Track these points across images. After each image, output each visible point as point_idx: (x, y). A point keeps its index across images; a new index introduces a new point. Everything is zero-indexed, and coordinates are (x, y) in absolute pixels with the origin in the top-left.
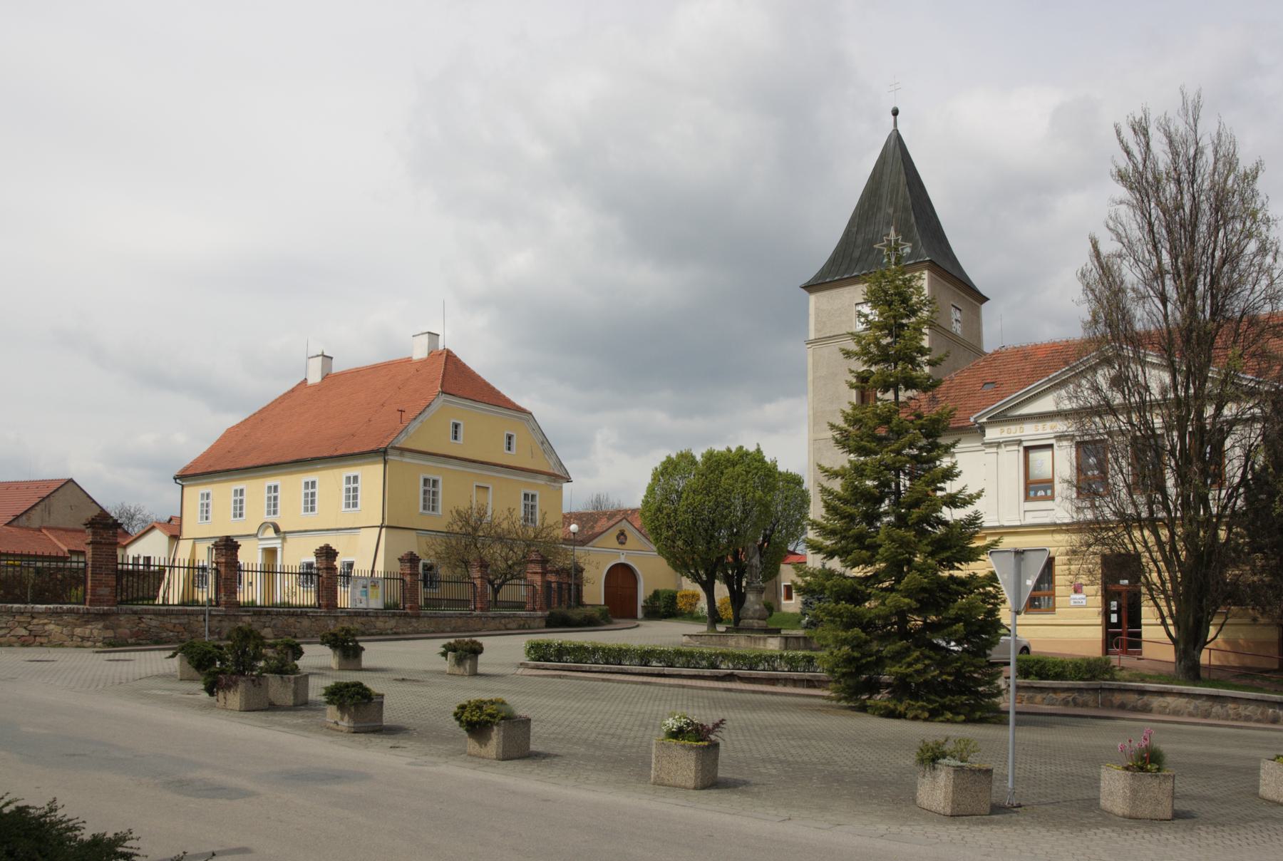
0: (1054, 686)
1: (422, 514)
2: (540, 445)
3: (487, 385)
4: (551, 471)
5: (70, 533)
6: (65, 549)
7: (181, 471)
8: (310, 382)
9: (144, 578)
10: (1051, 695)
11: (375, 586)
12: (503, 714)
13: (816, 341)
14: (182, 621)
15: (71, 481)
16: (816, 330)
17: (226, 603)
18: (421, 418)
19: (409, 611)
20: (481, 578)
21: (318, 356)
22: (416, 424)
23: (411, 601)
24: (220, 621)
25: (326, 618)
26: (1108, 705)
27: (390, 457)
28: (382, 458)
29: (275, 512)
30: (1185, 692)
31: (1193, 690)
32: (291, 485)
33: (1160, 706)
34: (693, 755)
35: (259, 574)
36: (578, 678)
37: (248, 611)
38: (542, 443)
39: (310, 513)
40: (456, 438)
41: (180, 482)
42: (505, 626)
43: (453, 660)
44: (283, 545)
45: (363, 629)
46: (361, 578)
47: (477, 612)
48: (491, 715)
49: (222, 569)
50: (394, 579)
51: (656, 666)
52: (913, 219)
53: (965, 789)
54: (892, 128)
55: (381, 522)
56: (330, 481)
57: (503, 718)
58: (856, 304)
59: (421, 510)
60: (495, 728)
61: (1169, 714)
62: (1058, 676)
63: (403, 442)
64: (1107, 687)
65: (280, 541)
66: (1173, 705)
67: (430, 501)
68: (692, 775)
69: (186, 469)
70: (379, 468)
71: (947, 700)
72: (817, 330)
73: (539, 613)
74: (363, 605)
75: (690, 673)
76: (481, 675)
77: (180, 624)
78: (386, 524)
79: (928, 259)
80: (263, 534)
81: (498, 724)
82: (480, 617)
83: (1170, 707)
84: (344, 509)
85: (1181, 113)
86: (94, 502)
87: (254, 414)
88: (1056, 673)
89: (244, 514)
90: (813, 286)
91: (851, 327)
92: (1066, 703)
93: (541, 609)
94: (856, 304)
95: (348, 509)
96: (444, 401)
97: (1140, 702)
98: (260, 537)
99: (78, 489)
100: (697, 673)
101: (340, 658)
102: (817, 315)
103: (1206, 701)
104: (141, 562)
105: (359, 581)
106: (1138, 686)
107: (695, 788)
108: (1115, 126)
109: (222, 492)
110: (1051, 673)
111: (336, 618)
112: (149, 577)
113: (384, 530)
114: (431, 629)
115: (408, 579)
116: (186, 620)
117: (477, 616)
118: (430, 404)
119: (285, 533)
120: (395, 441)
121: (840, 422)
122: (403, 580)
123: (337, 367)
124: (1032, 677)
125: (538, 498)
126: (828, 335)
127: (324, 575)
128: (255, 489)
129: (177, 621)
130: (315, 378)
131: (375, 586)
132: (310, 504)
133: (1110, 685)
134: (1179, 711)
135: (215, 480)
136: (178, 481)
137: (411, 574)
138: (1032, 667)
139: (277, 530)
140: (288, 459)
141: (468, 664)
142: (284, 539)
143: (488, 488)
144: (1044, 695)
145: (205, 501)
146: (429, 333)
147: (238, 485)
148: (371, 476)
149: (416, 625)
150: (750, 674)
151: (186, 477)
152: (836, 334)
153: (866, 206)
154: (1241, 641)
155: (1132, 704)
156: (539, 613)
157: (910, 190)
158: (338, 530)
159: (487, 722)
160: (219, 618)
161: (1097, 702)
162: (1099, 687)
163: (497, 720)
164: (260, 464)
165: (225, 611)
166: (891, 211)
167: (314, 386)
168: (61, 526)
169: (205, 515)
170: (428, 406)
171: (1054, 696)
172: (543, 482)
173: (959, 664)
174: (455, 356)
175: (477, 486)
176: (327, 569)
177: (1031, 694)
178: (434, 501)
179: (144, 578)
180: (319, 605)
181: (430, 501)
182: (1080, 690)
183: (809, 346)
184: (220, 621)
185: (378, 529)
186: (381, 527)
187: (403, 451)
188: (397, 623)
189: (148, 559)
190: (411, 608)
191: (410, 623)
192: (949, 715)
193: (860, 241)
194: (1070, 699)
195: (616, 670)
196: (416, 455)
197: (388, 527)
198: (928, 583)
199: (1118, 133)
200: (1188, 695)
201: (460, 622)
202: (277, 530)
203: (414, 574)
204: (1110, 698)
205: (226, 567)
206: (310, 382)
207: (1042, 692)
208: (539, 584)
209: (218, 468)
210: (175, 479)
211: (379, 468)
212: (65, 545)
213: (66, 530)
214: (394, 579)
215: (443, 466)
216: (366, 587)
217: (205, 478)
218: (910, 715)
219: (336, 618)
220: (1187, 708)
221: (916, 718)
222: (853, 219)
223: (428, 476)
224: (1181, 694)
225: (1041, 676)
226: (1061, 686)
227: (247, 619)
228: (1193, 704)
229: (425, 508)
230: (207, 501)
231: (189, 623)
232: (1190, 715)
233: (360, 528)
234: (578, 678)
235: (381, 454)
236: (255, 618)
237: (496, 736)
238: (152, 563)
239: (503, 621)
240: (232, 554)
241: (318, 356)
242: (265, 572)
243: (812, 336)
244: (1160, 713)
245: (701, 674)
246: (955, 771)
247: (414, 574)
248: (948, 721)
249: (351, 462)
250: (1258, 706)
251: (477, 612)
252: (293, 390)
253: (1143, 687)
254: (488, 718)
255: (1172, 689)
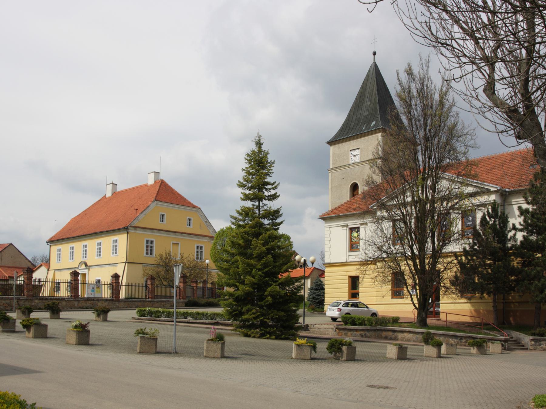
0: (355, 328)
1: (145, 256)
2: (205, 223)
3: (180, 196)
4: (211, 235)
5: (10, 269)
6: (7, 276)
7: (50, 239)
8: (107, 196)
9: (36, 288)
10: (355, 332)
11: (98, 288)
12: (35, 323)
13: (333, 169)
14: (7, 302)
15: (11, 244)
16: (333, 163)
17: (27, 295)
18: (145, 212)
19: (114, 299)
20: (151, 284)
21: (110, 184)
22: (143, 215)
23: (116, 294)
24: (25, 302)
25: (74, 301)
26: (380, 337)
27: (130, 231)
28: (126, 232)
29: (86, 257)
30: (411, 331)
31: (415, 330)
32: (92, 244)
33: (401, 337)
34: (75, 333)
35: (50, 283)
36: (164, 324)
37: (37, 298)
38: (206, 222)
39: (99, 257)
40: (163, 221)
41: (49, 244)
42: (164, 306)
43: (96, 315)
44: (89, 272)
45: (92, 306)
46: (92, 284)
47: (150, 299)
48: (31, 323)
49: (26, 281)
50: (138, 286)
51: (190, 319)
52: (378, 108)
53: (145, 344)
54: (373, 61)
55: (126, 260)
56: (107, 241)
57: (34, 324)
58: (351, 150)
59: (145, 254)
60: (32, 327)
61: (405, 341)
62: (360, 324)
63: (136, 224)
64: (379, 329)
65: (87, 270)
66: (407, 337)
67: (149, 250)
68: (75, 340)
69: (52, 238)
70: (125, 236)
71: (268, 330)
72: (333, 164)
73: (182, 300)
74: (92, 296)
75: (200, 322)
76: (109, 321)
77: (6, 303)
78: (128, 261)
79: (381, 127)
80: (81, 267)
81: (32, 326)
82: (151, 302)
83: (406, 338)
84: (112, 255)
85: (419, 66)
86: (22, 254)
87: (83, 212)
88: (359, 323)
89: (87, 257)
90: (332, 143)
91: (348, 162)
92: (362, 336)
93: (183, 298)
94: (351, 150)
95: (113, 255)
96: (156, 204)
97: (393, 335)
98: (79, 268)
99: (14, 248)
100: (203, 322)
101: (51, 314)
102: (333, 156)
103: (421, 335)
104: (37, 280)
105: (91, 285)
106: (392, 329)
107: (76, 345)
108: (397, 71)
109: (65, 248)
110: (357, 323)
111: (79, 301)
112: (38, 288)
113: (127, 264)
114: (125, 307)
115: (114, 284)
116: (9, 302)
117: (149, 301)
118: (149, 206)
119: (89, 266)
120: (132, 223)
121: (236, 215)
122: (112, 285)
123: (119, 188)
124: (349, 324)
125: (204, 248)
126: (338, 166)
127: (73, 283)
128: (78, 246)
129: (5, 302)
130: (109, 194)
131: (98, 288)
132: (99, 254)
133: (380, 328)
134: (409, 340)
135: (63, 243)
136: (48, 243)
137: (115, 283)
138: (348, 320)
139: (86, 265)
140: (90, 233)
141: (102, 316)
142: (89, 269)
143: (178, 244)
144: (352, 333)
145: (59, 253)
146: (155, 172)
147: (71, 245)
148: (122, 239)
149: (118, 305)
150: (225, 322)
151: (52, 241)
152: (341, 165)
153: (358, 102)
154: (481, 311)
155: (390, 337)
156: (182, 300)
157: (378, 93)
158: (109, 264)
159: (29, 325)
160: (24, 301)
161: (376, 336)
162: (376, 329)
163: (32, 324)
164: (80, 235)
165: (27, 298)
166: (369, 103)
167: (108, 198)
168: (7, 265)
169: (59, 259)
170: (148, 207)
171: (356, 333)
172: (206, 241)
173: (272, 315)
174: (166, 183)
175: (173, 243)
176: (74, 280)
177: (346, 332)
178: (151, 250)
179: (36, 288)
180: (71, 295)
181: (149, 250)
182: (368, 330)
183: (330, 171)
184: (25, 302)
185: (124, 264)
186: (126, 263)
187: (136, 228)
188: (108, 303)
189: (40, 279)
190: (115, 297)
191: (115, 304)
192: (268, 336)
193: (354, 119)
194: (364, 334)
195: (170, 320)
196: (142, 229)
197: (128, 263)
198: (511, 293)
199: (398, 74)
200: (413, 332)
201: (140, 304)
202: (86, 265)
203: (117, 283)
204: (381, 334)
205: (27, 280)
206: (107, 196)
207: (351, 331)
208: (182, 287)
209: (64, 237)
210: (47, 243)
211: (125, 236)
212: (7, 274)
213: (9, 267)
214: (138, 286)
215: (156, 234)
216: (94, 288)
217: (58, 242)
218: (252, 335)
219: (79, 301)
220: (413, 338)
221: (254, 337)
222: (352, 108)
223: (148, 239)
224: (410, 332)
225: (354, 324)
226: (359, 328)
227: (37, 301)
228: (415, 337)
229: (147, 253)
230: (60, 253)
231: (10, 302)
232: (414, 341)
233: (117, 263)
234: (164, 324)
235: (126, 229)
236: (40, 301)
237: (32, 330)
238: (41, 281)
239: (162, 303)
240: (30, 274)
241: (110, 184)
242: (82, 283)
243: (331, 167)
244: (402, 340)
245: (205, 322)
246: (141, 338)
247: (117, 283)
248: (267, 338)
249: (115, 234)
250: (445, 338)
251: (150, 299)
252: (100, 200)
253: (394, 329)
254: (30, 324)
255: (406, 330)
